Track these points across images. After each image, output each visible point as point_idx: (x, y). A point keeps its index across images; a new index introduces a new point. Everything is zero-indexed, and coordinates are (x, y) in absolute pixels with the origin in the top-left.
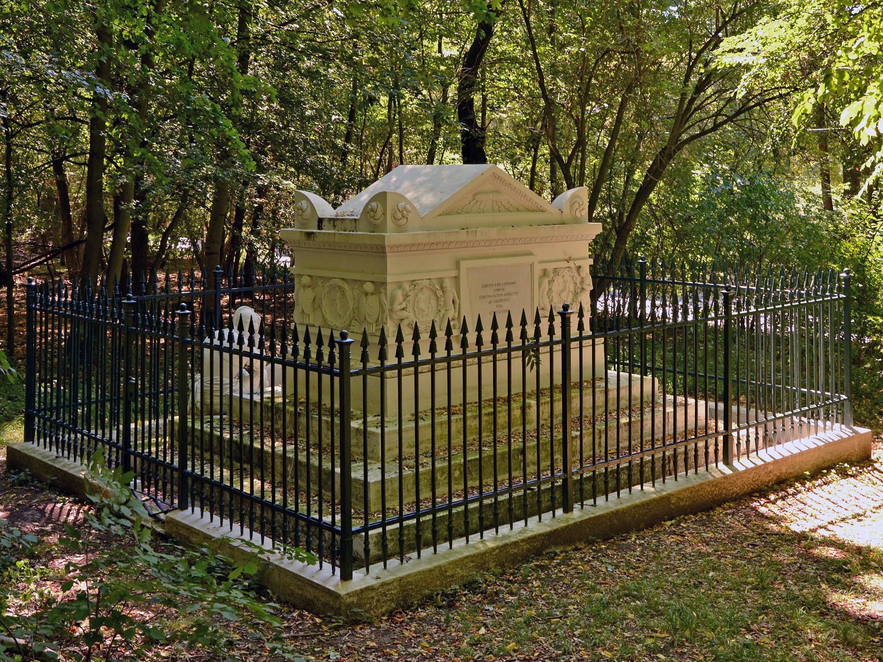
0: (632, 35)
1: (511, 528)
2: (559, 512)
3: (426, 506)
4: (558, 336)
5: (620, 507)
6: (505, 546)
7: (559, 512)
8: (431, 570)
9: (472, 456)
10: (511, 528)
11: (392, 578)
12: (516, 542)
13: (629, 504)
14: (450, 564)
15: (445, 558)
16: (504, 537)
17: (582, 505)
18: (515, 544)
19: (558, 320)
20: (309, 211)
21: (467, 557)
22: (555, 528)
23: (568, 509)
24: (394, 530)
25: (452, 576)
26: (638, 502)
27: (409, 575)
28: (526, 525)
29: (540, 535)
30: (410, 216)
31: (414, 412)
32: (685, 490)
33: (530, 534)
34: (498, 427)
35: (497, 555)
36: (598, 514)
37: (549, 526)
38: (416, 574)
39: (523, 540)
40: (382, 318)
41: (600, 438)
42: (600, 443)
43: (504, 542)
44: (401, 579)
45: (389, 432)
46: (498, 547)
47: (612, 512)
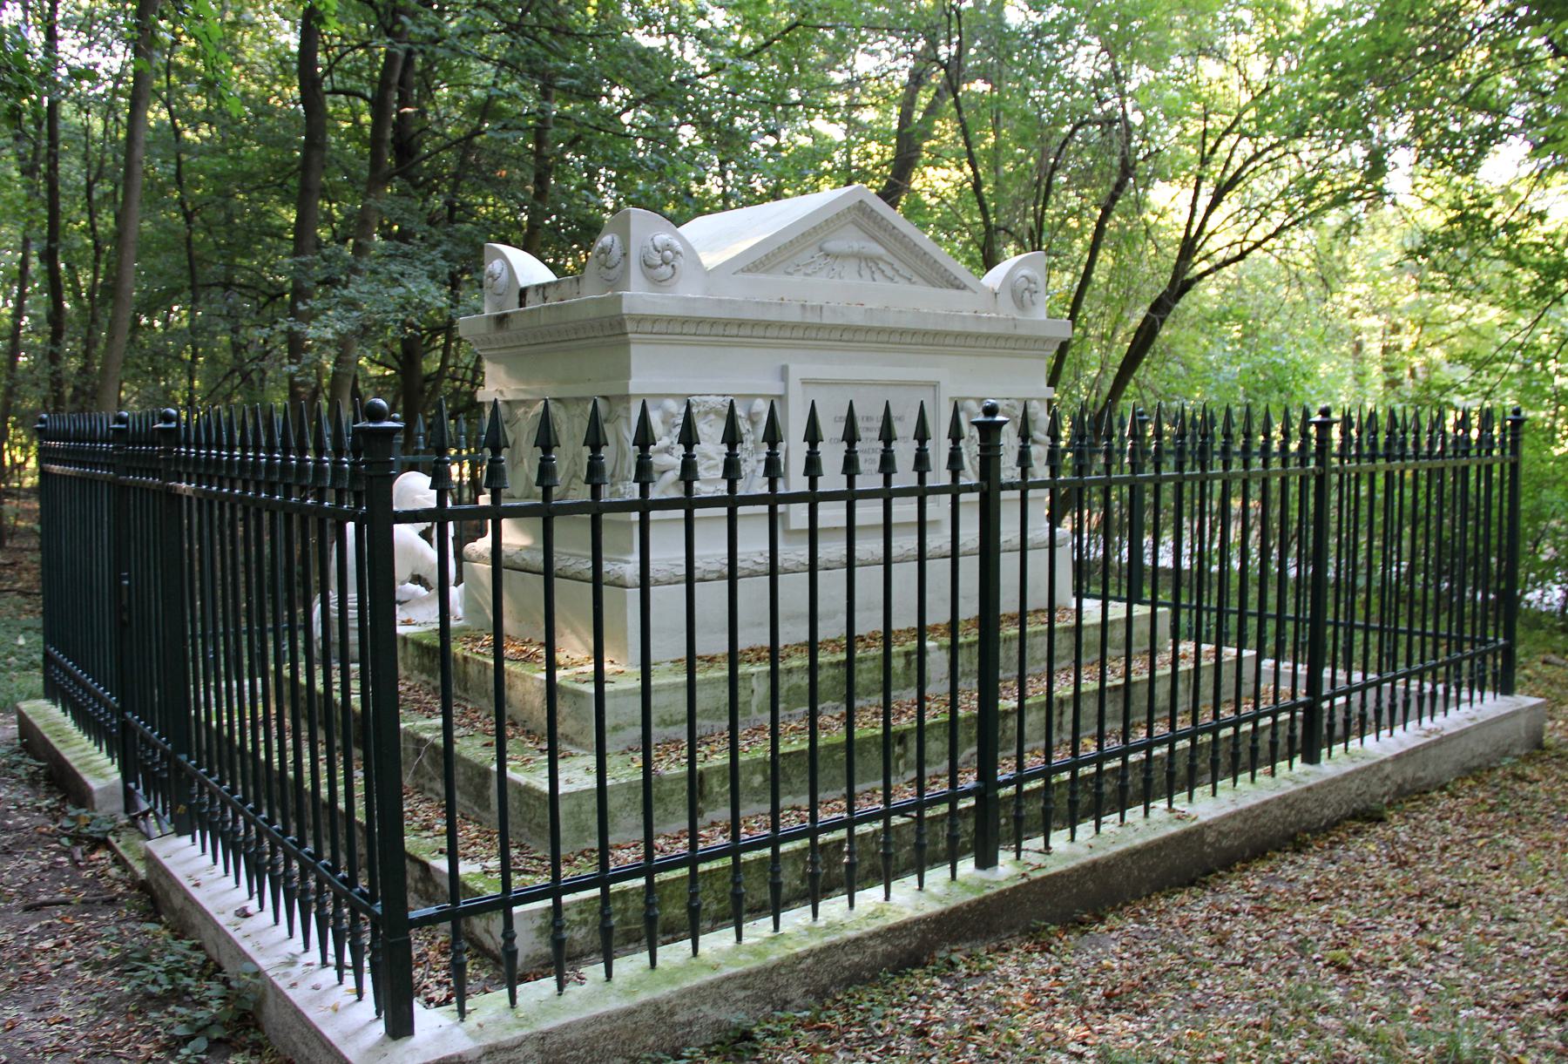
0: (947, 1021)
1: (851, 905)
2: (967, 866)
3: (626, 857)
4: (970, 476)
5: (1098, 855)
6: (830, 949)
7: (967, 866)
8: (630, 1013)
9: (792, 743)
10: (851, 905)
11: (518, 1033)
12: (857, 940)
13: (1120, 848)
14: (682, 995)
15: (672, 981)
16: (830, 927)
17: (1018, 851)
18: (857, 942)
19: (971, 437)
20: (505, 276)
21: (728, 979)
22: (952, 904)
23: (986, 861)
24: (586, 901)
25: (690, 1023)
26: (1138, 842)
27: (567, 1026)
28: (887, 898)
29: (917, 921)
30: (680, 263)
31: (683, 654)
32: (1232, 816)
33: (893, 919)
34: (858, 690)
35: (808, 969)
36: (1052, 871)
37: (940, 901)
38: (586, 1024)
39: (875, 935)
40: (622, 469)
41: (1061, 714)
42: (1060, 724)
43: (828, 939)
44: (544, 1036)
45: (616, 694)
46: (811, 953)
47: (1083, 867)
